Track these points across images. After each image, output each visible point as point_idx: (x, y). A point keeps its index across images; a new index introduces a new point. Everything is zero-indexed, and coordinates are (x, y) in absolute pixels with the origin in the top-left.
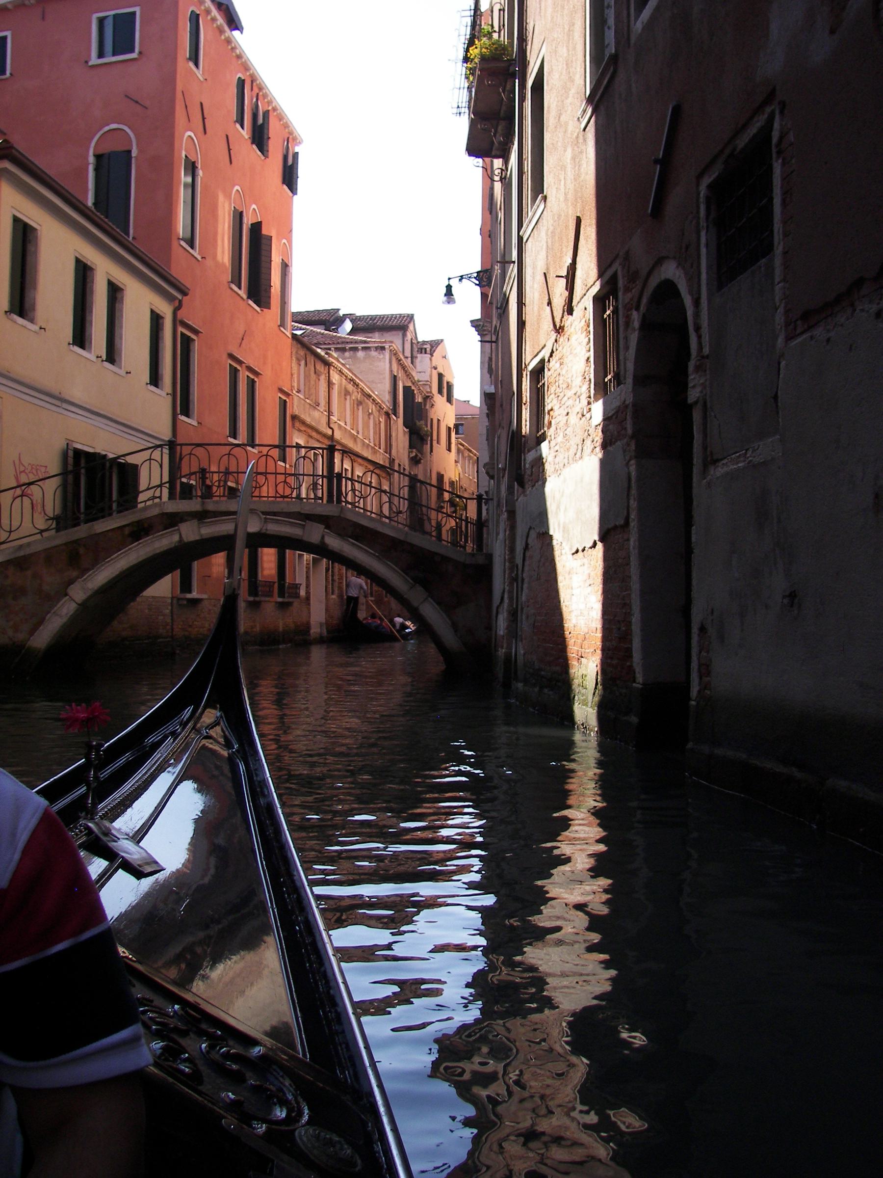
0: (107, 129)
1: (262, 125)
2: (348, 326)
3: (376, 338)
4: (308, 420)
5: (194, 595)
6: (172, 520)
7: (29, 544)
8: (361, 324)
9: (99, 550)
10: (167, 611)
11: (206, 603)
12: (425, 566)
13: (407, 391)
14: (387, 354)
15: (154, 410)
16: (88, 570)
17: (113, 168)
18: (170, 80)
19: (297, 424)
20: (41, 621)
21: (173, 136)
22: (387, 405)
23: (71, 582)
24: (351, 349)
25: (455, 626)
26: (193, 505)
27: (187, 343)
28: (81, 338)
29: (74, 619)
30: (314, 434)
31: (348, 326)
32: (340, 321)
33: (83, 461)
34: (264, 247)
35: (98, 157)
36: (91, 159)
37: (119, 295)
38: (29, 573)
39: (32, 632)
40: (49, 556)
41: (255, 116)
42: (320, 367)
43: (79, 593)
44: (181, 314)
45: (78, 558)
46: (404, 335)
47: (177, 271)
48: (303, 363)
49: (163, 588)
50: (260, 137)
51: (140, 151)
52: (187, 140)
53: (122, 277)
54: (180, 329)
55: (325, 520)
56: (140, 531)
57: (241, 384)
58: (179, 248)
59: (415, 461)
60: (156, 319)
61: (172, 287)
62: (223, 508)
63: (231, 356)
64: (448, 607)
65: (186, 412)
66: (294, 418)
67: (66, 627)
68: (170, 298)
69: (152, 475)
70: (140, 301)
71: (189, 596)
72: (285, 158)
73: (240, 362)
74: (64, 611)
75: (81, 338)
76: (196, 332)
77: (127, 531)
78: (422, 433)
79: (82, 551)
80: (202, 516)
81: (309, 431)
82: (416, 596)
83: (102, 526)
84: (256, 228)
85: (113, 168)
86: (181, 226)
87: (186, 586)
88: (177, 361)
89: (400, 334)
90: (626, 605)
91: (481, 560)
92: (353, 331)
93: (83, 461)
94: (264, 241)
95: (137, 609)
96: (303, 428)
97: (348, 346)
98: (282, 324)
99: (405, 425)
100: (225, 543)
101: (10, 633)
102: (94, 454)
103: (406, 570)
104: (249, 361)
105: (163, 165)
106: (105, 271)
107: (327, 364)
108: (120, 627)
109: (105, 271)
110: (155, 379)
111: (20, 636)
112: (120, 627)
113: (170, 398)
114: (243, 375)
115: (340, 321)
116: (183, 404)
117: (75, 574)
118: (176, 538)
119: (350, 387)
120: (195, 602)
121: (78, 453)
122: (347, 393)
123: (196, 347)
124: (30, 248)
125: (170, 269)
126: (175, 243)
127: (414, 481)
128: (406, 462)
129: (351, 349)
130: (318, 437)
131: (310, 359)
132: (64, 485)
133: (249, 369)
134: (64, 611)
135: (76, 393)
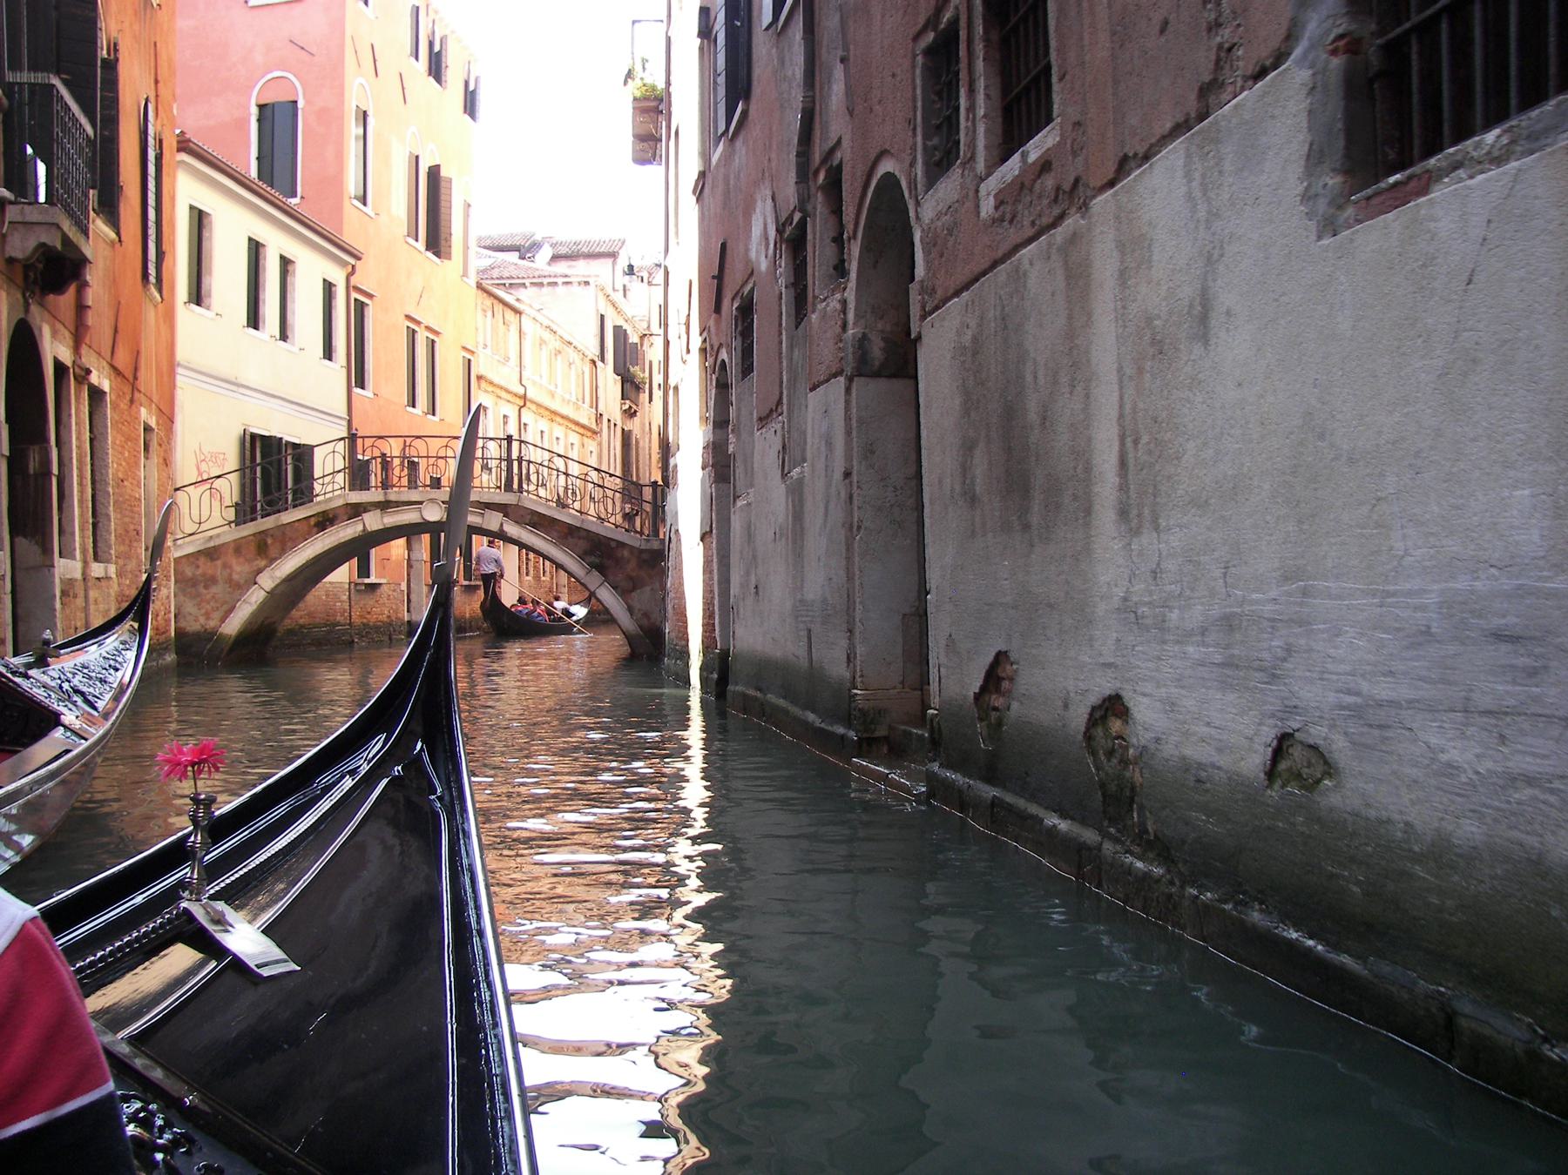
0: (269, 76)
1: (439, 53)
2: (545, 253)
3: (581, 268)
4: (496, 380)
5: (373, 579)
6: (356, 511)
7: (218, 535)
8: (563, 250)
9: (286, 540)
10: (345, 598)
11: (384, 589)
12: (598, 552)
13: (620, 333)
14: (592, 287)
15: (328, 382)
16: (276, 559)
17: (276, 122)
18: (338, 26)
19: (483, 384)
20: (232, 609)
21: (342, 87)
22: (594, 351)
23: (260, 571)
24: (550, 284)
25: (630, 610)
26: (374, 495)
27: (360, 307)
28: (254, 320)
29: (263, 606)
30: (503, 394)
31: (545, 253)
32: (535, 246)
33: (258, 445)
34: (443, 191)
35: (261, 107)
36: (254, 111)
37: (290, 268)
38: (219, 563)
39: (223, 620)
40: (238, 547)
41: (431, 44)
42: (510, 315)
43: (270, 579)
44: (354, 281)
45: (265, 548)
46: (614, 263)
47: (349, 236)
48: (489, 314)
49: (342, 575)
50: (436, 69)
51: (307, 102)
52: (358, 89)
53: (294, 249)
54: (354, 295)
55: (503, 509)
56: (325, 521)
57: (420, 346)
58: (351, 208)
59: (630, 414)
60: (329, 287)
61: (348, 254)
62: (404, 498)
63: (408, 317)
64: (624, 592)
65: (361, 384)
66: (479, 378)
67: (254, 615)
68: (343, 264)
69: (328, 464)
70: (313, 269)
71: (367, 581)
72: (467, 84)
73: (418, 323)
74: (253, 599)
75: (254, 320)
76: (370, 296)
77: (313, 521)
78: (637, 381)
79: (269, 541)
80: (384, 506)
81: (498, 391)
82: (594, 580)
83: (289, 517)
84: (434, 172)
85: (276, 122)
86: (352, 185)
87: (364, 570)
88: (350, 336)
89: (610, 261)
90: (712, 591)
91: (655, 545)
92: (556, 258)
93: (258, 445)
94: (443, 184)
95: (316, 597)
96: (490, 389)
97: (545, 281)
98: (465, 274)
99: (616, 372)
100: (408, 532)
101: (202, 620)
102: (270, 437)
103: (582, 556)
104: (426, 321)
105: (331, 117)
106: (277, 243)
107: (518, 312)
108: (299, 615)
109: (277, 243)
110: (328, 353)
111: (212, 624)
112: (299, 615)
113: (344, 371)
114: (422, 337)
115: (535, 246)
116: (358, 376)
117: (263, 563)
118: (360, 527)
119: (547, 335)
120: (373, 587)
121: (254, 437)
122: (542, 342)
123: (370, 314)
124: (205, 234)
125: (341, 230)
126: (346, 204)
127: (626, 437)
128: (617, 416)
129: (550, 284)
130: (509, 397)
131: (499, 308)
132: (243, 477)
133: (428, 328)
134: (253, 599)
135: (251, 377)
